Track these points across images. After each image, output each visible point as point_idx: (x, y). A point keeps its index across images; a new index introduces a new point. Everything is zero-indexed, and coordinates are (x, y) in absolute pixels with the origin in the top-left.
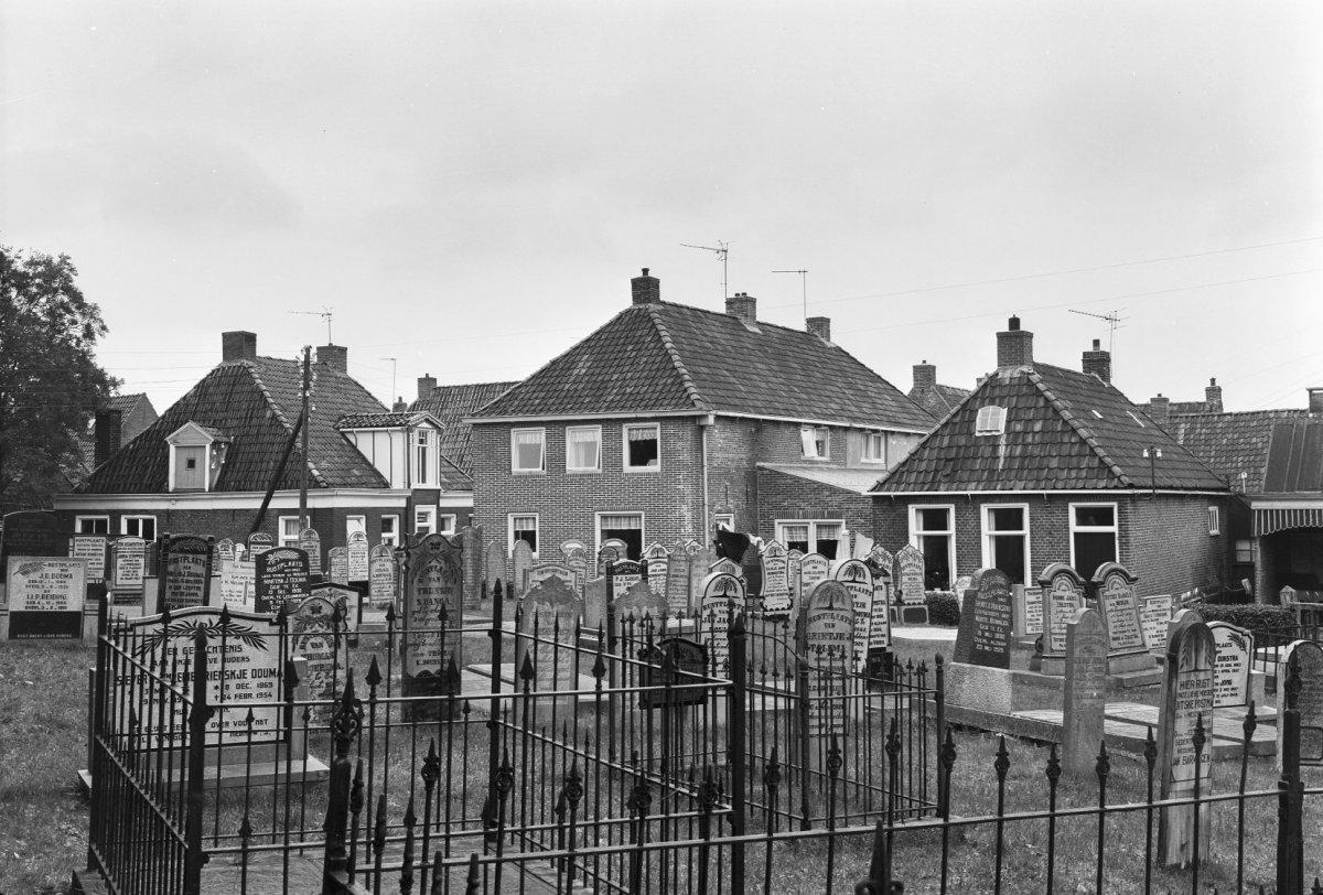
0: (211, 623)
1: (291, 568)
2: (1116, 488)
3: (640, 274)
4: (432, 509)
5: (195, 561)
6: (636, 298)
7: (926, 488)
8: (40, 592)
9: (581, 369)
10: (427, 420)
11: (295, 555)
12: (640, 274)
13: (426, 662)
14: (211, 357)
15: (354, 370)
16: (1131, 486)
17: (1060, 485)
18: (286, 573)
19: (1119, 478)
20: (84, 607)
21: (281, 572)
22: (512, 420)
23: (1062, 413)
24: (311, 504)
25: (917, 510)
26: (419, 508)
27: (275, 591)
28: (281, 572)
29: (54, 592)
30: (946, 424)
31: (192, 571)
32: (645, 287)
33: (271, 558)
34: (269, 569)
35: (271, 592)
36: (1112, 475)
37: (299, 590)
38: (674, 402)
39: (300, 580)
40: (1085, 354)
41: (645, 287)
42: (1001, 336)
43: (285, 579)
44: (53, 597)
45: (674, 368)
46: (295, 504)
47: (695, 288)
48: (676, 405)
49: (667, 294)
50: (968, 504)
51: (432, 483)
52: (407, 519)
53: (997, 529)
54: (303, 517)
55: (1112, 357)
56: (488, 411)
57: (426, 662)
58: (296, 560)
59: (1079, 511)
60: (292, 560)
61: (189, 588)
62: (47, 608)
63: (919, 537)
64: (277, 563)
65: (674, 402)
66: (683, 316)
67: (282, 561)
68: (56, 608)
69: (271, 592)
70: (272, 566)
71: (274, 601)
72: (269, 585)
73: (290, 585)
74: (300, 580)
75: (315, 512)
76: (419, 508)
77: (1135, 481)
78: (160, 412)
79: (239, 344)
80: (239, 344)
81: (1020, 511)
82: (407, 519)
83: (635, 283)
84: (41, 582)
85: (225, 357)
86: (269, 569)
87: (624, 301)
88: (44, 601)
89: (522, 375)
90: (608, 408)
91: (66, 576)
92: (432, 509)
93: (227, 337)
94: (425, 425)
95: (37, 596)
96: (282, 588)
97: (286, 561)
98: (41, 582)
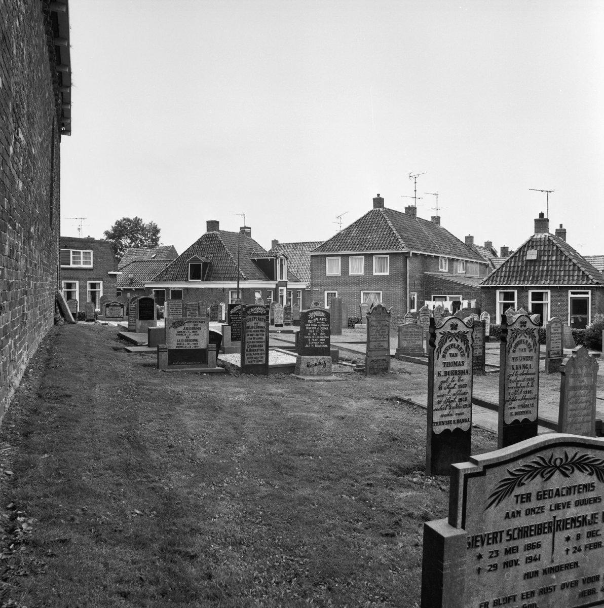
0: (567, 457)
1: (321, 321)
2: (591, 284)
3: (376, 196)
4: (284, 289)
5: (260, 320)
6: (375, 206)
7: (505, 283)
8: (184, 338)
9: (353, 234)
10: (283, 255)
11: (323, 314)
12: (376, 196)
13: (516, 414)
14: (203, 231)
15: (254, 236)
16: (597, 283)
17: (575, 282)
18: (318, 324)
19: (592, 280)
20: (208, 346)
21: (315, 323)
22: (327, 254)
23: (565, 253)
24: (241, 286)
25: (500, 292)
26: (280, 288)
27: (312, 334)
28: (315, 323)
29: (192, 337)
30: (513, 257)
31: (258, 325)
32: (378, 202)
33: (311, 315)
34: (309, 321)
35: (309, 334)
36: (588, 279)
37: (324, 334)
38: (395, 247)
39: (325, 328)
40: (557, 230)
41: (378, 202)
42: (536, 221)
43: (317, 327)
44: (190, 340)
45: (393, 233)
46: (235, 286)
47: (396, 203)
48: (396, 248)
49: (387, 205)
50: (523, 290)
51: (284, 279)
52: (276, 292)
53: (504, 300)
54: (238, 290)
55: (486, 241)
56: (314, 251)
57: (516, 414)
58: (323, 317)
59: (533, 293)
60: (321, 317)
61: (257, 335)
62: (188, 347)
63: (501, 303)
64: (314, 318)
65: (395, 247)
66: (392, 213)
67: (316, 317)
68: (193, 347)
69: (309, 334)
70: (311, 319)
71: (311, 339)
72: (309, 330)
73: (320, 331)
74: (325, 328)
75: (243, 289)
76: (280, 288)
77: (600, 282)
78: (180, 254)
79: (213, 225)
80: (213, 225)
81: (514, 293)
82: (276, 292)
83: (374, 199)
84: (184, 332)
85: (207, 231)
86: (309, 321)
87: (370, 207)
88: (186, 343)
89: (325, 238)
90: (367, 249)
91: (198, 328)
92: (284, 289)
93: (208, 222)
94: (282, 256)
95: (182, 340)
96: (315, 332)
97: (319, 317)
98: (184, 332)
